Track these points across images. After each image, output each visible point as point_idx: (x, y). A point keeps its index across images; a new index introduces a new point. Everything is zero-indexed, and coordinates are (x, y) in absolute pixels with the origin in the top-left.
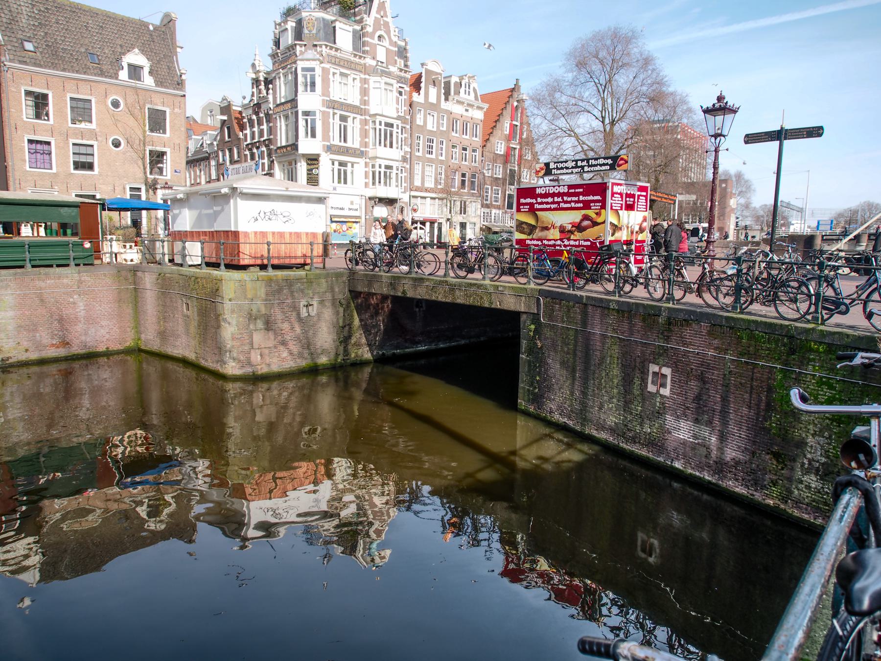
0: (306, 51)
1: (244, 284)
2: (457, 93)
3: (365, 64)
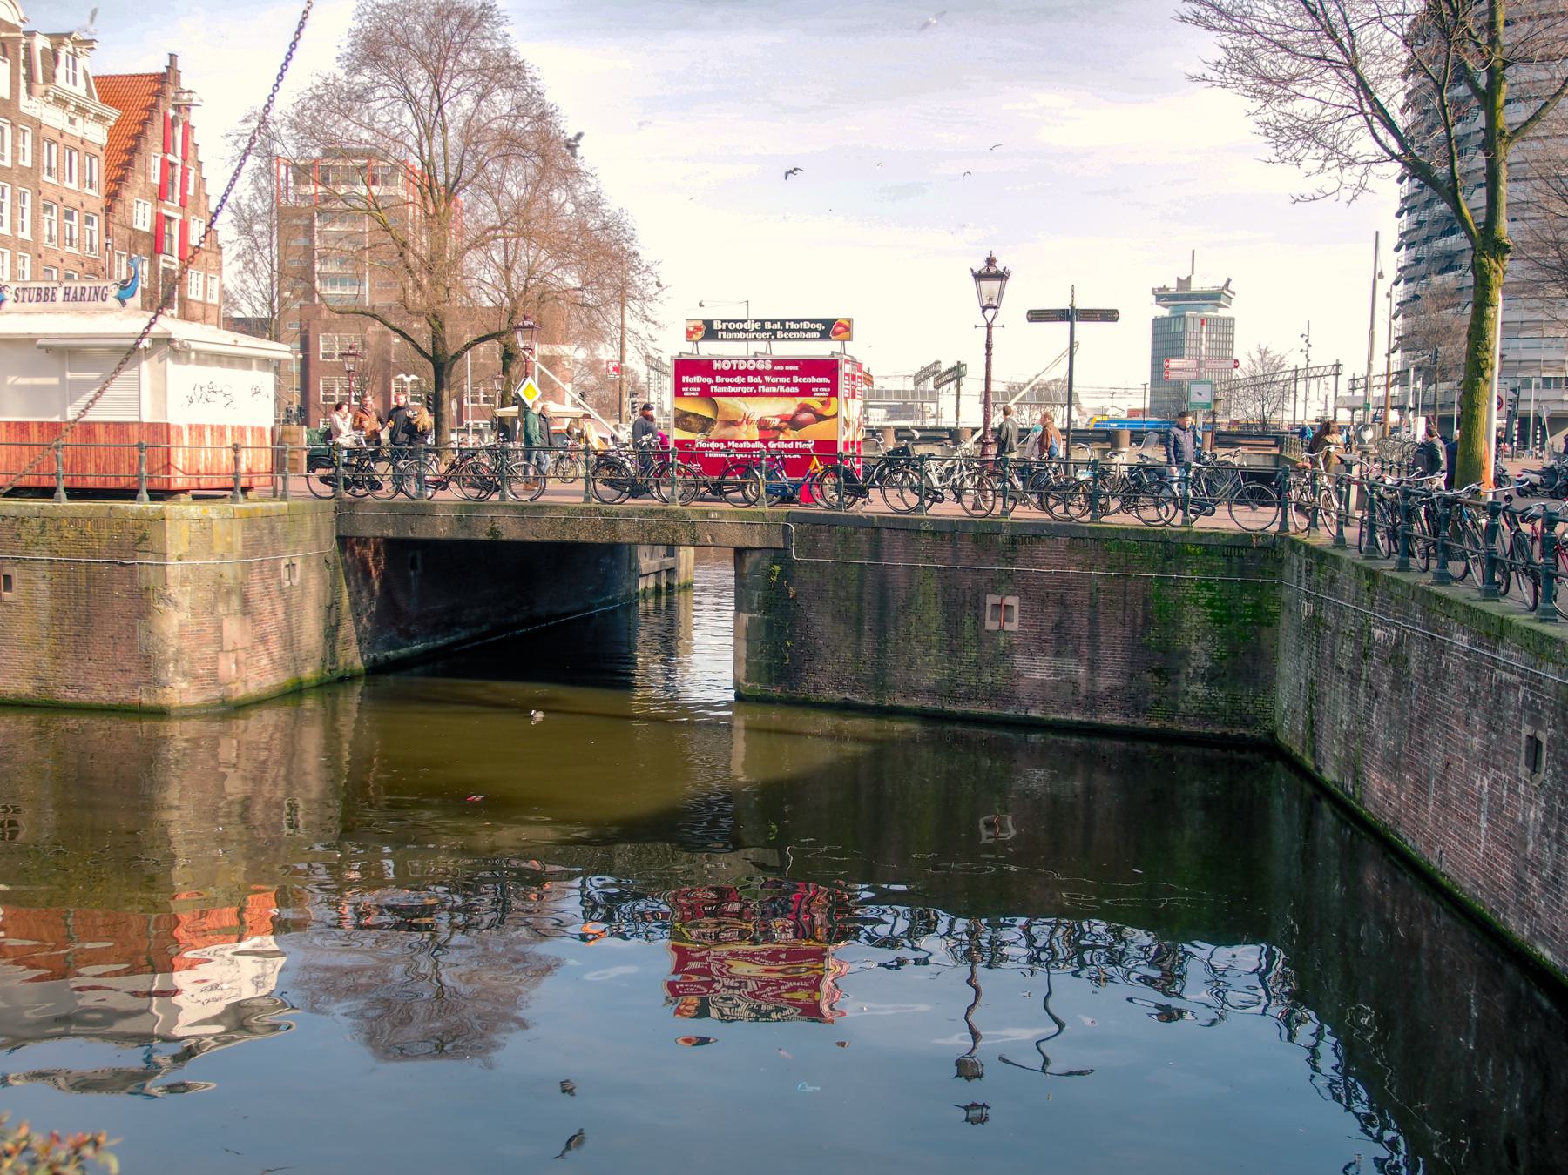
1: (207, 525)
2: (50, 77)
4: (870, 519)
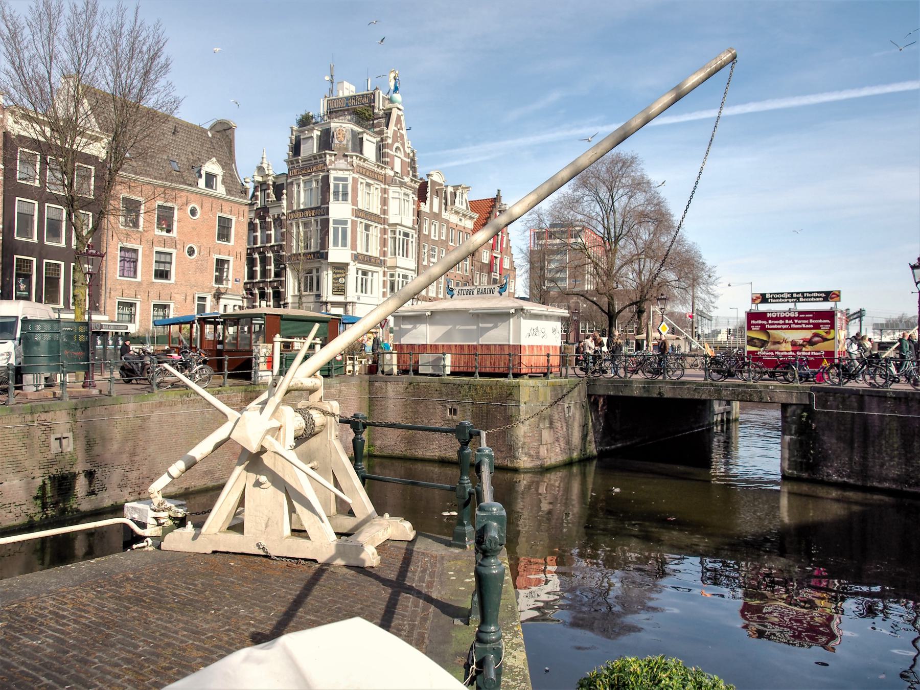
0: (336, 160)
2: (453, 203)
3: (385, 174)
4: (858, 391)
